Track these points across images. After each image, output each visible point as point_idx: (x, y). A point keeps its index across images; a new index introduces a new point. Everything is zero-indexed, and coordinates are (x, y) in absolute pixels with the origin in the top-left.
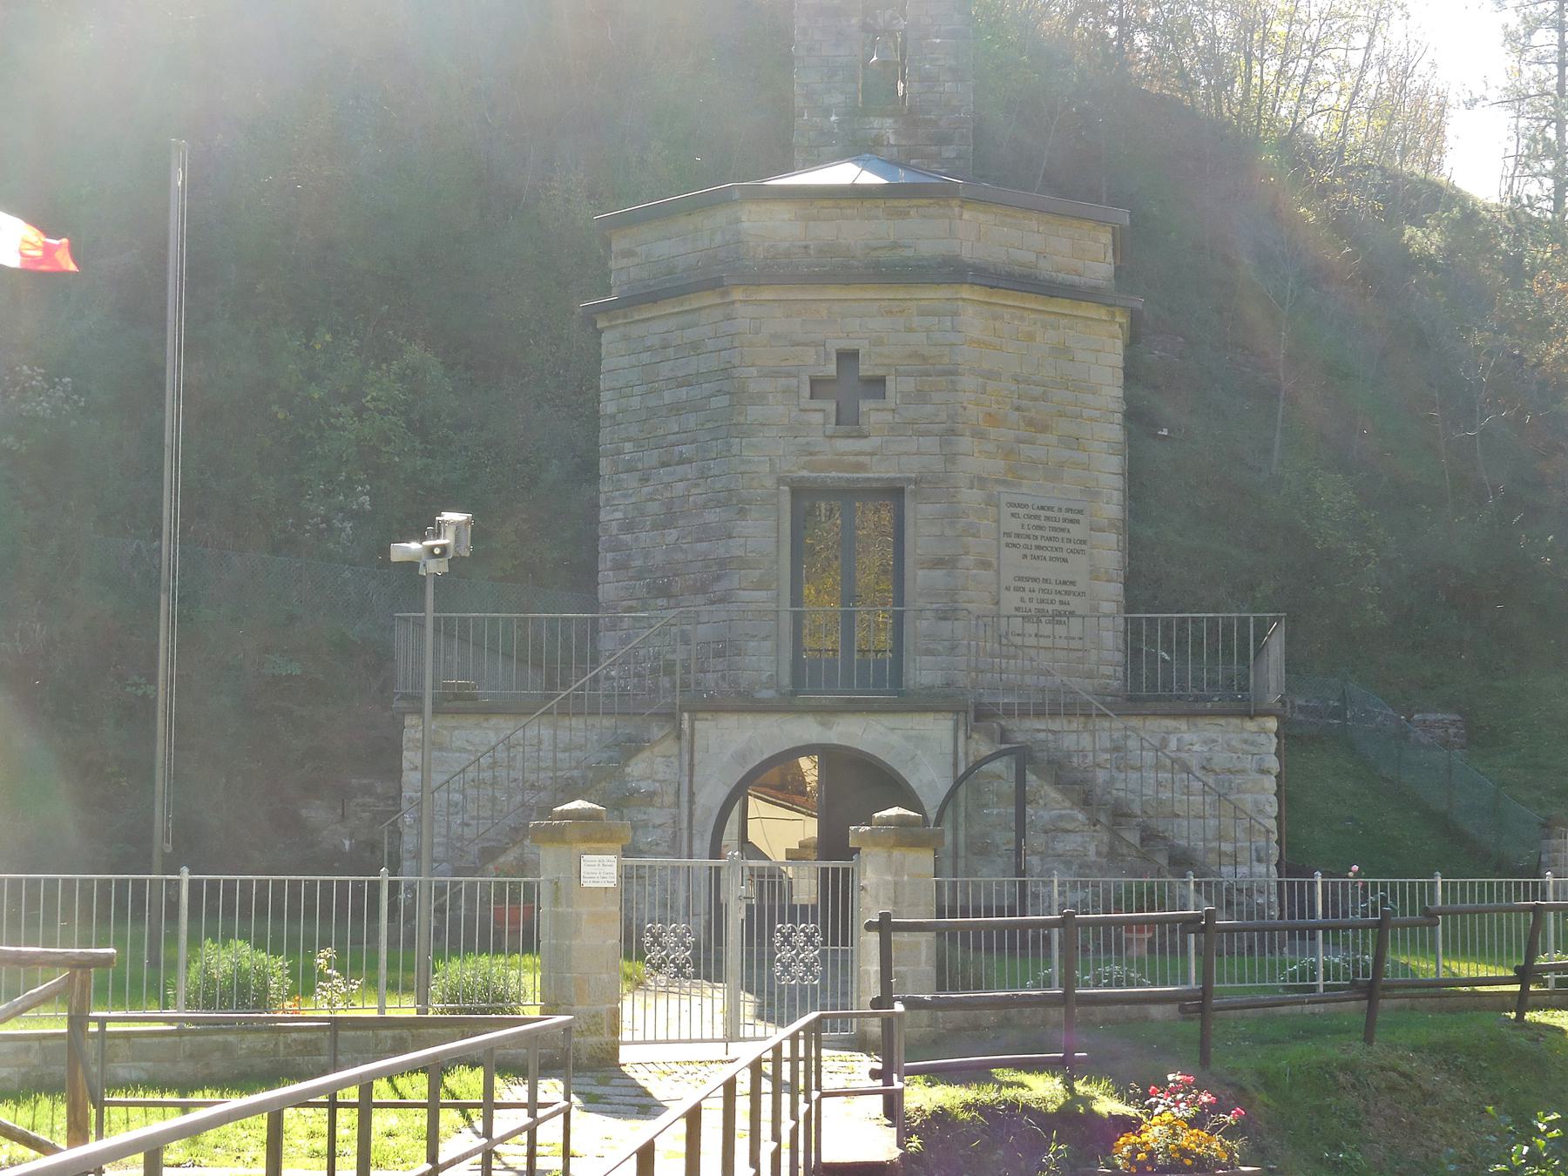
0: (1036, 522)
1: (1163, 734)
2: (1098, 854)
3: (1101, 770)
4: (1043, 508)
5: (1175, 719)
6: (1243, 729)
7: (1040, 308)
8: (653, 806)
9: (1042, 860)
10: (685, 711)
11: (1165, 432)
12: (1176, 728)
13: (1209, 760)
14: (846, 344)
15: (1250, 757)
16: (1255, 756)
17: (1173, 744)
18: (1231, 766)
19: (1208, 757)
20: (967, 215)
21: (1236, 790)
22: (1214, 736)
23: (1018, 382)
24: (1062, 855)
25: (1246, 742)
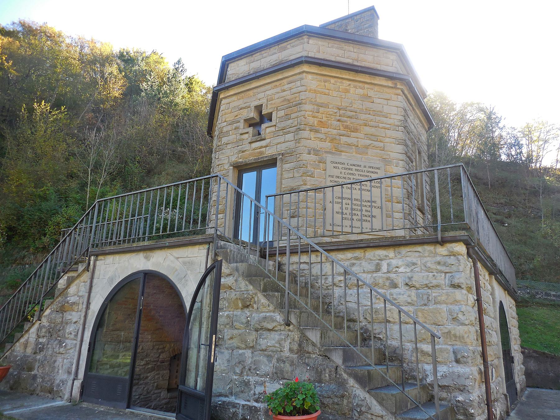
0: (350, 172)
1: (377, 261)
2: (291, 350)
3: (337, 288)
4: (354, 165)
5: (385, 249)
6: (436, 254)
7: (352, 78)
8: (74, 311)
9: (252, 353)
10: (92, 255)
11: (507, 225)
12: (386, 256)
13: (410, 278)
14: (257, 103)
15: (443, 275)
16: (447, 275)
17: (384, 268)
18: (427, 282)
19: (410, 276)
20: (311, 41)
21: (433, 302)
22: (415, 260)
23: (340, 109)
24: (265, 350)
25: (439, 263)
